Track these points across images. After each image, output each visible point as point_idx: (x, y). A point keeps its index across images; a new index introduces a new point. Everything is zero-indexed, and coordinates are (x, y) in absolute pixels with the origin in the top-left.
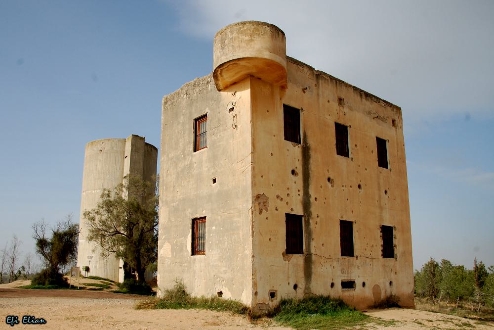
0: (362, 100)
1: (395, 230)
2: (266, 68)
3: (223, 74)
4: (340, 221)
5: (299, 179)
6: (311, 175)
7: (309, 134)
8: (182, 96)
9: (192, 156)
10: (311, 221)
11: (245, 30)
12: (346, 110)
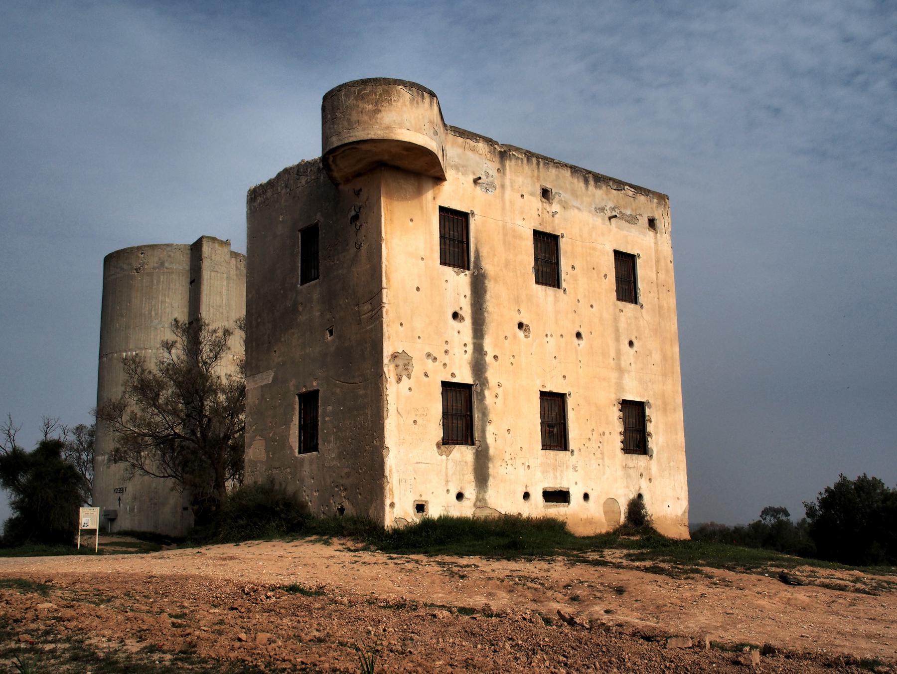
1: (650, 408)
5: (466, 326)
7: (484, 252)
10: (487, 393)
12: (556, 207)
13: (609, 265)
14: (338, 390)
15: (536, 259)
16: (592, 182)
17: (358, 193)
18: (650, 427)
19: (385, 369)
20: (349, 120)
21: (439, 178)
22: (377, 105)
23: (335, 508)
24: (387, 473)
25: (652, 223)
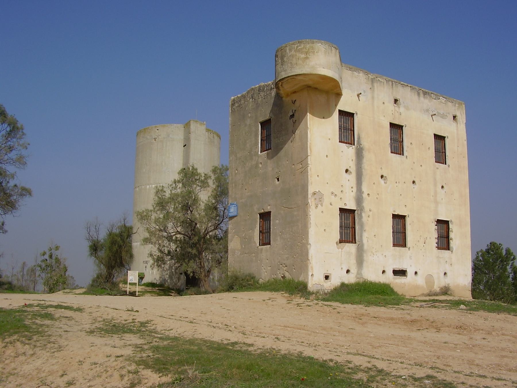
0: (419, 99)
1: (452, 224)
3: (284, 85)
4: (393, 215)
5: (352, 177)
7: (363, 136)
8: (248, 99)
10: (363, 215)
11: (302, 49)
12: (402, 110)
13: (431, 142)
14: (282, 212)
15: (391, 139)
17: (294, 102)
18: (451, 235)
19: (309, 201)
20: (291, 63)
21: (339, 95)
22: (307, 54)
23: (280, 276)
24: (310, 258)
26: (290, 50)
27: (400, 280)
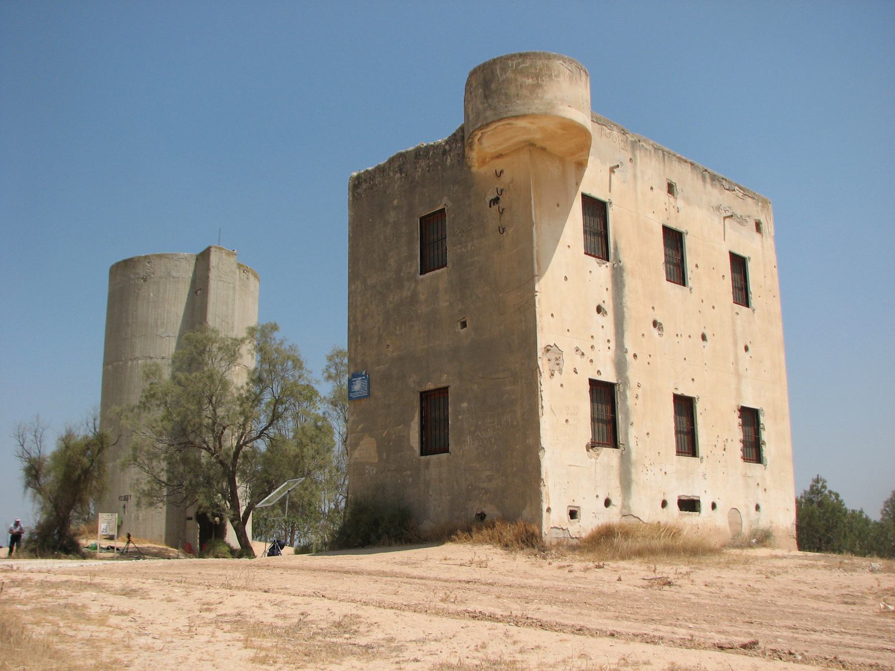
2: (560, 131)
3: (484, 140)
5: (608, 321)
6: (627, 315)
7: (622, 245)
8: (391, 174)
9: (416, 281)
10: (628, 393)
12: (680, 203)
15: (666, 255)
16: (708, 180)
17: (499, 175)
18: (764, 436)
19: (540, 363)
20: (506, 94)
22: (537, 79)
24: (543, 476)
25: (758, 226)
26: (504, 70)
27: (690, 519)
